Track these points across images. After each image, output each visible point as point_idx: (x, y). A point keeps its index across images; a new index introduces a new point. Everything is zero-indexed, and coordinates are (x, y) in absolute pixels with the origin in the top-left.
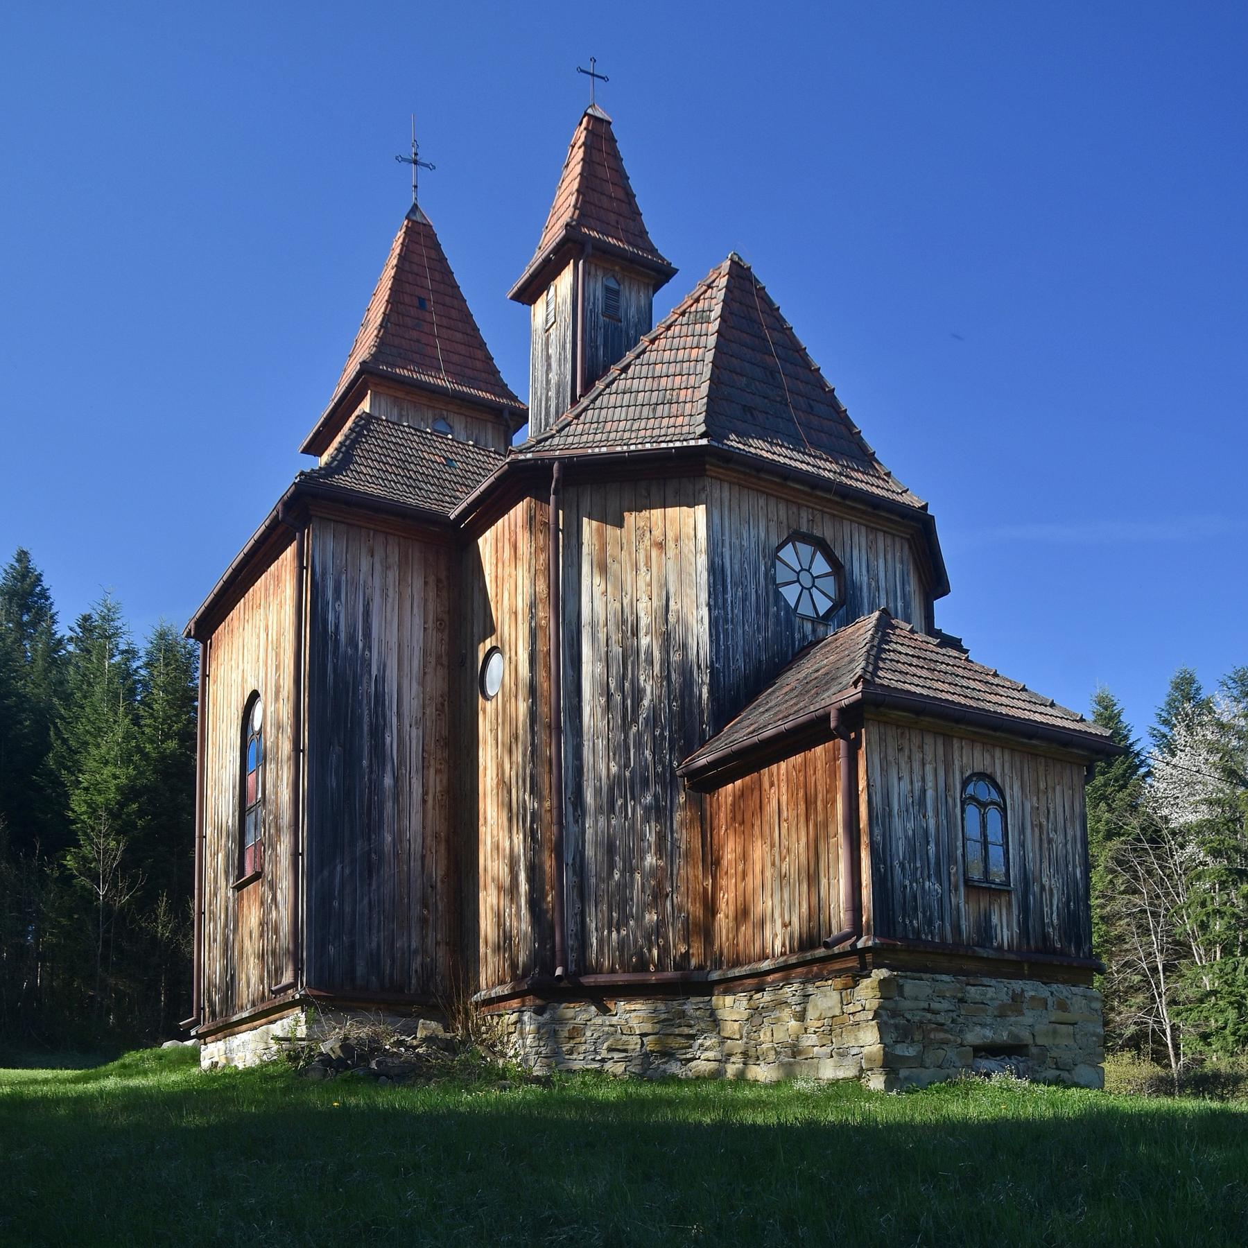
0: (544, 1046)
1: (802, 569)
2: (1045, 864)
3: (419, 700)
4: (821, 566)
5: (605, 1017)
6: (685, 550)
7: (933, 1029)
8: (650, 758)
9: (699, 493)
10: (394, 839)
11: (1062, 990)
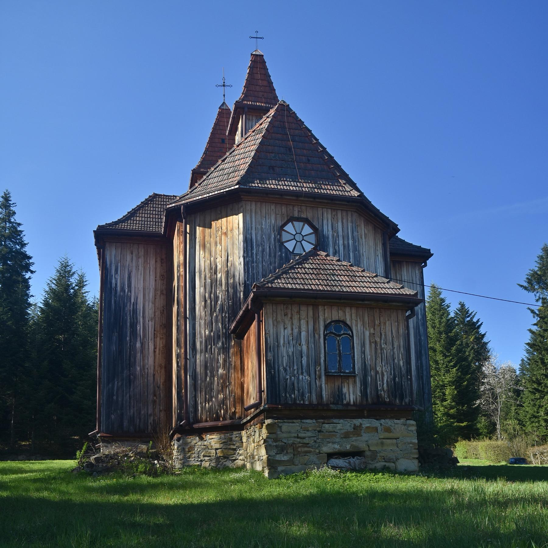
0: (180, 455)
1: (297, 233)
2: (379, 360)
3: (152, 310)
4: (307, 230)
5: (202, 442)
6: (235, 234)
7: (300, 447)
8: (220, 326)
9: (240, 208)
10: (141, 369)
11: (388, 422)
